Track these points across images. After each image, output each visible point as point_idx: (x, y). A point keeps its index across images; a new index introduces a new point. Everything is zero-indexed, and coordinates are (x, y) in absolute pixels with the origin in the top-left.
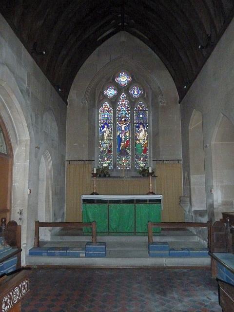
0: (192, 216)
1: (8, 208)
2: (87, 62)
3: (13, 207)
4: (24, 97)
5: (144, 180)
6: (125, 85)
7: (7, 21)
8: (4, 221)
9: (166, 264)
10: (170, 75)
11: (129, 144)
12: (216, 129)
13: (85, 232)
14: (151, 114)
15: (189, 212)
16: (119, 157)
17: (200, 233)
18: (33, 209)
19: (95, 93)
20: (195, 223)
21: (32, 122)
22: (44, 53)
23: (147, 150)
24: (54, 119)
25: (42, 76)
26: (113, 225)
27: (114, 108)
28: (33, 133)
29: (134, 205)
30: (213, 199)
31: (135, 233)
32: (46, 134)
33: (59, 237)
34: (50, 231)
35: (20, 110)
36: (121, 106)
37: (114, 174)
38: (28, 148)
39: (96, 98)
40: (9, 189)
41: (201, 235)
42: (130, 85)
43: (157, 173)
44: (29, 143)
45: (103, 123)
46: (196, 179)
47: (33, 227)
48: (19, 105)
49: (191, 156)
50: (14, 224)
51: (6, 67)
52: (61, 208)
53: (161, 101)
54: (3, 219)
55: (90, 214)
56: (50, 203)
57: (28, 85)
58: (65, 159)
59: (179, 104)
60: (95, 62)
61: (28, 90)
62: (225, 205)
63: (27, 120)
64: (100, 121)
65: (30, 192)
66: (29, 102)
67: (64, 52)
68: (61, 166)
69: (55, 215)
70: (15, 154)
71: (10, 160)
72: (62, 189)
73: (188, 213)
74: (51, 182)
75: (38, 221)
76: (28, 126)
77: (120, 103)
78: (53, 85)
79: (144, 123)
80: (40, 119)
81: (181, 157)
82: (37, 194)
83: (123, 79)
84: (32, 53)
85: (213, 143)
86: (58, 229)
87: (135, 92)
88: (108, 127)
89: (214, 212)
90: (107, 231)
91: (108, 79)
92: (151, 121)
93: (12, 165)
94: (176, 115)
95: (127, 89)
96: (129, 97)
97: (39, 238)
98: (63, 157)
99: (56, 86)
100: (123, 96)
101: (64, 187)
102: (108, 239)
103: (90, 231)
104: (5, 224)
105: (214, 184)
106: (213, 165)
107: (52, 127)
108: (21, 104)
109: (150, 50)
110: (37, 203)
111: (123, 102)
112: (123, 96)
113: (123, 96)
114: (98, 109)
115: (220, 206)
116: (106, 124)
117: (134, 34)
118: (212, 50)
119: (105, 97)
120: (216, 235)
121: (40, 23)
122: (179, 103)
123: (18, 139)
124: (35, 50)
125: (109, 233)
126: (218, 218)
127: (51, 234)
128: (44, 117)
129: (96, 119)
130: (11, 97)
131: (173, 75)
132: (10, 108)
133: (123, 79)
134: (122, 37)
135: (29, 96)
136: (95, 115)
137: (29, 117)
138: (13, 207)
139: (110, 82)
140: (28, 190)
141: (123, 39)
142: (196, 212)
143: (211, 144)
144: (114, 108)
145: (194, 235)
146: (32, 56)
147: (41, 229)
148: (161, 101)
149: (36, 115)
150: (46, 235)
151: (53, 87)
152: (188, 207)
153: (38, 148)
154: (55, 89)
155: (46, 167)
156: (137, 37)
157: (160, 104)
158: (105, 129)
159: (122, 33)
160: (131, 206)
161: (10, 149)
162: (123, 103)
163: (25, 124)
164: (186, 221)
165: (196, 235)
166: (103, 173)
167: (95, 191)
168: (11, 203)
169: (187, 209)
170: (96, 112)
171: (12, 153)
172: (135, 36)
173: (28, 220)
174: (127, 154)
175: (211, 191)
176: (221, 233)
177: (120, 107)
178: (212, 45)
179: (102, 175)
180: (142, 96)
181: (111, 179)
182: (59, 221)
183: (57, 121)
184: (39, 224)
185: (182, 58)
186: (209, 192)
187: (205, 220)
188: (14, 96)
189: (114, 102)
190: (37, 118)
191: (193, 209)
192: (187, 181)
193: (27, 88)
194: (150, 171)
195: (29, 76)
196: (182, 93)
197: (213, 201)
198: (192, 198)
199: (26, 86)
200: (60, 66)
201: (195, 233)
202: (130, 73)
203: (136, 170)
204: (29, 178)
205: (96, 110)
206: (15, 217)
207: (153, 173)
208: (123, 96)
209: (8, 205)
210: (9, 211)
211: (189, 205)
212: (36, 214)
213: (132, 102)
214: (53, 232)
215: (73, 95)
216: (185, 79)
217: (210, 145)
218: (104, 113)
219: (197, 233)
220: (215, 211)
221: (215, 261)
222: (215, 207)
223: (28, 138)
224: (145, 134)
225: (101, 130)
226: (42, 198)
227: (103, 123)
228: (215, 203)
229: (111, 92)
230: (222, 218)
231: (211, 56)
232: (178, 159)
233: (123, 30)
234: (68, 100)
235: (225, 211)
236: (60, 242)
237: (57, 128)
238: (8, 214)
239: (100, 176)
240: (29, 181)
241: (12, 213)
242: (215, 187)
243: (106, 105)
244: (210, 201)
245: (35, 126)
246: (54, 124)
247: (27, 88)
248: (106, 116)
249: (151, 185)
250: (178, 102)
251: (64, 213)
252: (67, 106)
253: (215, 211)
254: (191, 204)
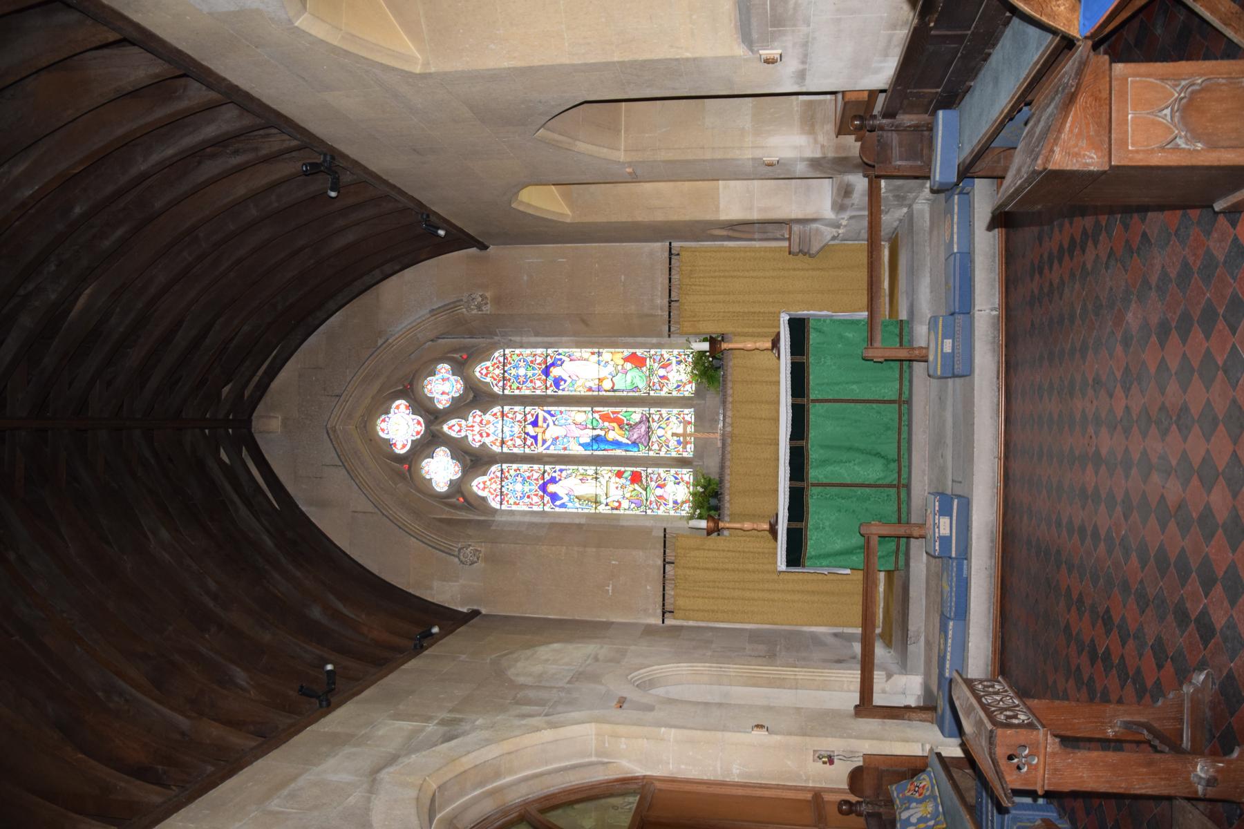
0: (851, 218)
1: (809, 796)
2: (341, 539)
3: (807, 780)
4: (465, 733)
5: (735, 368)
6: (419, 423)
7: (250, 763)
8: (847, 808)
9: (994, 309)
10: (394, 277)
11: (614, 413)
12: (582, 146)
13: (897, 562)
14: (518, 339)
15: (838, 226)
16: (656, 447)
17: (904, 198)
18: (817, 722)
19: (441, 520)
20: (871, 214)
21: (539, 715)
22: (329, 667)
23: (634, 354)
24: (529, 652)
25: (393, 680)
26: (873, 472)
27: (493, 459)
28: (576, 715)
29: (811, 405)
30: (795, 160)
31: (903, 403)
32: (579, 676)
33: (911, 648)
34: (889, 676)
35: (506, 746)
36: (488, 435)
37: (712, 465)
38: (621, 729)
39: (460, 514)
40: (748, 792)
41: (911, 196)
42: (423, 407)
43: (713, 329)
44: (607, 727)
45: (542, 498)
46: (734, 201)
47: (871, 724)
48: (493, 746)
49: (659, 217)
50: (856, 777)
51: (384, 775)
52: (816, 640)
53: (479, 308)
54: (841, 811)
55: (839, 545)
56: (802, 674)
57: (428, 719)
58: (655, 625)
59: (492, 249)
60: (343, 517)
61: (443, 723)
62: (813, 126)
63: (538, 729)
64: (535, 508)
65: (762, 727)
66: (480, 722)
67: (316, 613)
68: (674, 632)
69: (839, 661)
70: (640, 771)
71: (658, 785)
72: (755, 637)
73: (841, 231)
74: (733, 669)
75: (856, 707)
76: (553, 726)
77: (478, 438)
78: (419, 649)
79: (546, 362)
80: (532, 694)
81: (659, 248)
82: (769, 708)
83: (399, 427)
84: (422, 646)
85: (622, 156)
86: (880, 651)
87: (442, 386)
88: (553, 480)
89: (835, 158)
90: (894, 490)
91: (401, 476)
92: (539, 339)
93: (673, 780)
94: (529, 260)
95: (432, 416)
96: (459, 408)
97: (908, 708)
98: (649, 631)
99: (422, 642)
100: (456, 428)
101: (750, 631)
102: (921, 484)
103: (892, 546)
104: (858, 802)
105: (748, 155)
106: (690, 157)
107: (554, 660)
108: (488, 742)
109: (312, 339)
110: (798, 709)
111: (481, 428)
112: (452, 428)
113: (456, 428)
114: (495, 511)
115: (816, 141)
116: (543, 488)
117: (263, 388)
118: (345, 157)
119: (458, 488)
120: (901, 159)
121: (241, 676)
122: (486, 248)
123: (594, 759)
124: (322, 696)
125: (902, 486)
126: (852, 145)
127: (901, 673)
128: (521, 680)
129: (527, 519)
130: (467, 767)
131: (397, 268)
132: (498, 775)
133: (399, 427)
134: (270, 427)
135: (461, 720)
136: (511, 524)
137: (524, 722)
138: (807, 780)
139: (410, 468)
140: (756, 732)
141: (275, 424)
142: (839, 207)
143: (624, 163)
144: (493, 459)
145: (910, 215)
146: (339, 705)
147: (878, 700)
148: (479, 308)
149: (518, 702)
150: (902, 686)
151: (426, 652)
152: (823, 228)
153: (621, 703)
154: (430, 645)
155: (683, 677)
156: (272, 380)
157: (488, 309)
158: (561, 493)
159: (258, 424)
160: (815, 413)
161: (624, 786)
162: (477, 428)
163: (548, 735)
164: (864, 234)
165: (910, 206)
166: (710, 499)
167: (766, 526)
168: (796, 789)
169: (828, 232)
170: (504, 519)
171: (636, 778)
172: (268, 385)
173: (850, 737)
174: (647, 420)
175: (770, 165)
176: (895, 143)
177: (492, 438)
178: (333, 158)
179: (713, 502)
180: (461, 368)
181: (727, 478)
182: (857, 648)
183: (535, 646)
184: (866, 707)
185: (339, 236)
186: (776, 172)
187: (860, 183)
188: (464, 760)
189: (474, 460)
190: (529, 702)
191: (828, 213)
192: (739, 229)
193: (438, 724)
194: (705, 346)
195: (398, 717)
196: (460, 240)
197: (803, 159)
198: (793, 216)
199: (431, 727)
200: (348, 624)
201: (905, 210)
202: (381, 406)
203: (698, 393)
204: (716, 729)
205: (498, 518)
206: (836, 778)
207: (712, 341)
208: (452, 428)
209: (801, 796)
210: (817, 795)
211: (814, 226)
212: (835, 714)
213: (477, 398)
214: (894, 668)
215: (446, 592)
216: (410, 231)
217: (630, 164)
218: (508, 493)
219: (901, 206)
220: (831, 154)
221: (980, 166)
222: (818, 155)
223: (590, 729)
224: (581, 359)
225: (563, 506)
226: (785, 697)
227: (542, 498)
228: (809, 154)
229: (440, 470)
230: (853, 137)
231: (364, 163)
232: (667, 254)
233: (250, 421)
234: (465, 610)
235: (830, 128)
236: (928, 643)
237: (556, 646)
238: (827, 797)
239: (717, 508)
240: (725, 729)
241: (824, 785)
242: (758, 153)
243: (483, 486)
244: (801, 168)
245: (547, 703)
246: (544, 652)
247: (438, 724)
248: (518, 487)
249: (747, 525)
250: (483, 253)
251: (836, 635)
252: (484, 611)
253: (831, 154)
254: (814, 220)
